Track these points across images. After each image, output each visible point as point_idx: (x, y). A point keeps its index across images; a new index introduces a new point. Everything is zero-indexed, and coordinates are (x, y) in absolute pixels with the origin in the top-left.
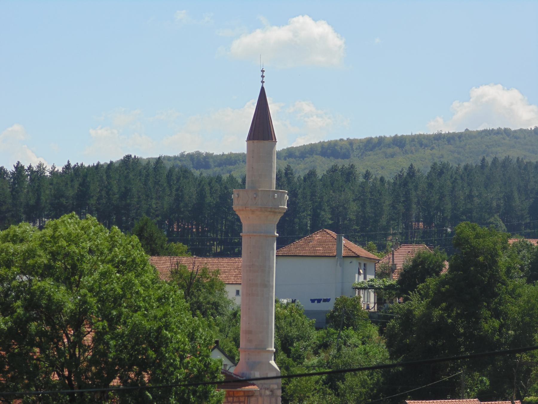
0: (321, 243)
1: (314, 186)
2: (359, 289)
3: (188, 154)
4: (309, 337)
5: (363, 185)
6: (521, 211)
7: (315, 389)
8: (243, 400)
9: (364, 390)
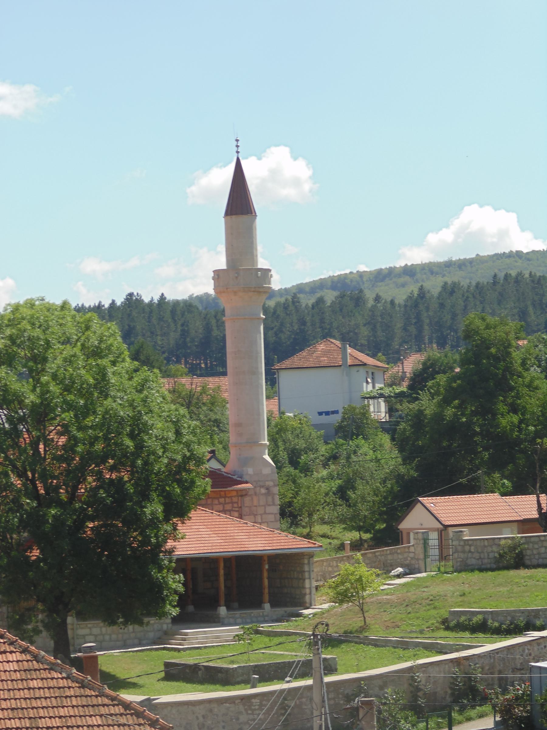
0: (325, 353)
1: (323, 313)
2: (367, 398)
3: (197, 296)
4: (317, 449)
5: (373, 309)
6: (537, 325)
7: (325, 502)
8: (236, 501)
9: (378, 499)
